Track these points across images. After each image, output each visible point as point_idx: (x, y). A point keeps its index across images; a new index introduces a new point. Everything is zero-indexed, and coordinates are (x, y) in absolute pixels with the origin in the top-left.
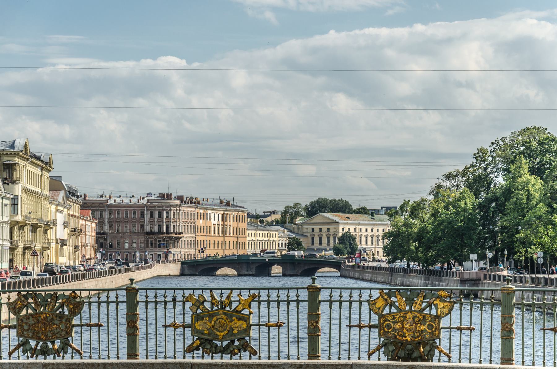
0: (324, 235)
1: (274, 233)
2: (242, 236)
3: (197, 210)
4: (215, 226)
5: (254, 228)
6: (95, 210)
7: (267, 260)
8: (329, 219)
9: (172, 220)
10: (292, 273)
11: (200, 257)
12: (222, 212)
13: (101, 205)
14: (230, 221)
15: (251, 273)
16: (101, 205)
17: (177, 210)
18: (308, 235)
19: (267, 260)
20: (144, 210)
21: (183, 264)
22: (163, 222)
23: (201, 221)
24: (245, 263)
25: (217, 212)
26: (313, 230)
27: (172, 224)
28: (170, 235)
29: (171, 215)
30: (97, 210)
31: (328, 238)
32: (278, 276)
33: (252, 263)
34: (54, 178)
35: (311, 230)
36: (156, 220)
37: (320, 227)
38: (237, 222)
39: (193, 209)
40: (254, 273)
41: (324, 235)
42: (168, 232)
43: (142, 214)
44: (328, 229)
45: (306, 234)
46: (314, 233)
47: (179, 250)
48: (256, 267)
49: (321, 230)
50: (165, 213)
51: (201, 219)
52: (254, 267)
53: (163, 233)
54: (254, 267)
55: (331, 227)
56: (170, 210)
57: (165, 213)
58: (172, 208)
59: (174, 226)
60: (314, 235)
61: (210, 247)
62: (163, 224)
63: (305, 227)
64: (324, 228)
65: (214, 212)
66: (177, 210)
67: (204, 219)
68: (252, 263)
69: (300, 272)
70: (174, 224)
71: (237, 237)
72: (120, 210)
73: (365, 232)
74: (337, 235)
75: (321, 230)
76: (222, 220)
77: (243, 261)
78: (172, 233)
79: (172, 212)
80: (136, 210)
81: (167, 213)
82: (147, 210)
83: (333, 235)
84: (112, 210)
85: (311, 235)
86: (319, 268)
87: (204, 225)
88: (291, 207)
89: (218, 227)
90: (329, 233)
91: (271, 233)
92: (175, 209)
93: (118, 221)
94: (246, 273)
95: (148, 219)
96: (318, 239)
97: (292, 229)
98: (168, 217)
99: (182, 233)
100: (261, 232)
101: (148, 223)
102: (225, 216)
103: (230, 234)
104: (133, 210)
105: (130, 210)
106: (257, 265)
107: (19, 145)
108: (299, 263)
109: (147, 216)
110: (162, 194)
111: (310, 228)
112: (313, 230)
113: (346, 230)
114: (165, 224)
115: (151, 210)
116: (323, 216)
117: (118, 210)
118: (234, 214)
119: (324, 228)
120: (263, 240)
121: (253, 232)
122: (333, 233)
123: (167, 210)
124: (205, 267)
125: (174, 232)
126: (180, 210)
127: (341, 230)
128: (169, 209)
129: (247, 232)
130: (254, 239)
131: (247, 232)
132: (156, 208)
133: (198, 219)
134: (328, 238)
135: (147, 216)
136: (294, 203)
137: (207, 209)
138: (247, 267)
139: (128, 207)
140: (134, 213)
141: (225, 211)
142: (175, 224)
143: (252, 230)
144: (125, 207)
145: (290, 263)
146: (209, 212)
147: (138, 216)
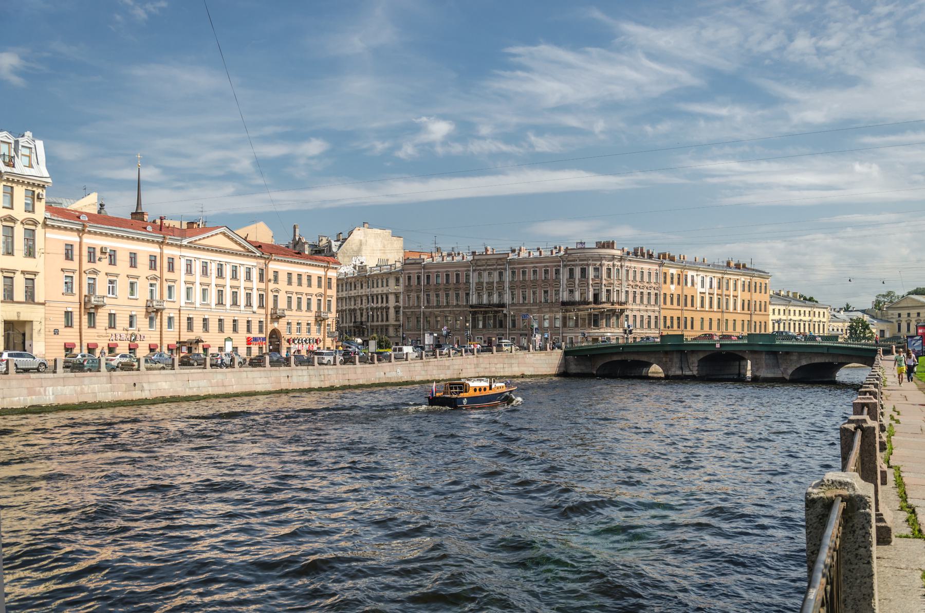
1: (822, 311)
2: (672, 307)
3: (664, 269)
4: (703, 295)
5: (784, 302)
6: (491, 269)
7: (718, 346)
8: (919, 301)
9: (604, 282)
10: (770, 375)
12: (720, 276)
13: (500, 262)
14: (735, 290)
15: (688, 373)
16: (500, 262)
17: (614, 265)
18: (894, 320)
19: (718, 346)
20: (560, 266)
21: (566, 353)
22: (588, 284)
23: (673, 287)
24: (678, 351)
25: (707, 274)
26: (899, 315)
27: (604, 289)
28: (601, 306)
29: (602, 274)
30: (495, 269)
33: (693, 352)
36: (577, 282)
37: (900, 312)
38: (749, 291)
39: (656, 267)
40: (695, 373)
42: (608, 301)
43: (557, 272)
45: (891, 320)
48: (700, 361)
49: (909, 315)
50: (591, 269)
51: (672, 283)
52: (694, 360)
53: (589, 303)
54: (696, 361)
56: (601, 265)
57: (591, 269)
58: (604, 262)
59: (608, 291)
61: (692, 328)
62: (588, 288)
63: (890, 312)
64: (913, 312)
65: (702, 274)
66: (614, 265)
67: (679, 283)
68: (693, 352)
69: (790, 372)
70: (609, 288)
71: (751, 314)
72: (525, 268)
75: (909, 315)
76: (719, 288)
78: (604, 303)
79: (604, 269)
80: (548, 266)
81: (596, 269)
82: (565, 266)
84: (515, 268)
87: (680, 293)
88: (884, 296)
89: (711, 298)
91: (817, 310)
92: (611, 263)
93: (524, 285)
94: (679, 373)
95: (565, 282)
97: (874, 314)
98: (596, 277)
99: (625, 303)
100: (797, 309)
101: (565, 286)
102: (725, 281)
103: (711, 307)
104: (545, 267)
105: (541, 268)
106: (701, 356)
107: (699, 260)
108: (787, 353)
109: (564, 276)
110: (600, 242)
114: (591, 289)
115: (569, 265)
116: (912, 299)
117: (523, 268)
118: (743, 279)
120: (801, 320)
121: (782, 308)
123: (595, 265)
124: (607, 360)
125: (608, 301)
126: (621, 266)
128: (598, 263)
129: (771, 308)
130: (784, 318)
131: (771, 308)
132: (577, 262)
133: (665, 282)
135: (564, 276)
137: (684, 268)
138: (681, 361)
139: (537, 263)
140: (546, 272)
141: (725, 274)
142: (611, 288)
143: (779, 305)
144: (532, 263)
145: (768, 353)
146: (690, 273)
147: (552, 275)
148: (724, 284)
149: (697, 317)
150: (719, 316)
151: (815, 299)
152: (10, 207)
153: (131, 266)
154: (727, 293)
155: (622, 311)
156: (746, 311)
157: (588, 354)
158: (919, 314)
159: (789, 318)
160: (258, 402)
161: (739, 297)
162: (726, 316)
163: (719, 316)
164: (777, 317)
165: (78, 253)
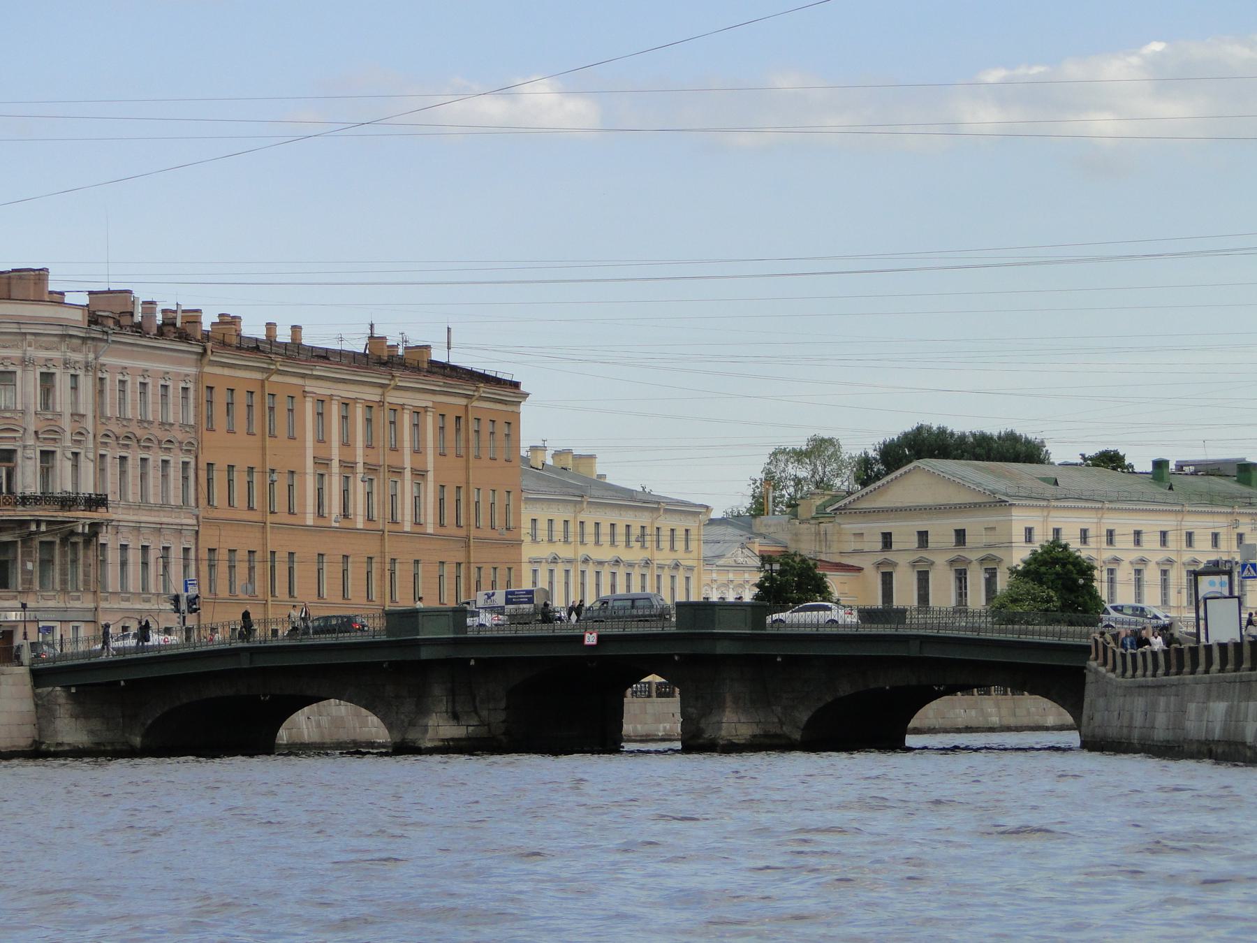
0: (940, 560)
2: (230, 514)
7: (590, 639)
11: (1244, 659)
18: (866, 563)
19: (590, 639)
26: (887, 539)
31: (961, 576)
32: (988, 749)
34: (461, 97)
35: (914, 542)
37: (959, 522)
41: (940, 560)
44: (960, 535)
46: (889, 555)
47: (87, 602)
55: (974, 525)
60: (894, 564)
73: (1157, 545)
74: (1001, 561)
77: (721, 648)
83: (982, 561)
85: (879, 565)
86: (929, 695)
88: (799, 456)
90: (924, 554)
96: (951, 578)
111: (874, 529)
112: (887, 539)
113: (1042, 538)
119: (941, 530)
122: (982, 554)
127: (1018, 535)
130: (565, 552)
134: (961, 576)
136: (810, 434)
148: (1174, 661)
149: (306, 548)
150: (371, 547)
151: (495, 425)
152: (1207, 600)
153: (890, 534)
154: (391, 459)
155: (95, 527)
156: (451, 529)
157: (122, 678)
158: (960, 535)
159: (582, 552)
160: (292, 616)
161: (430, 476)
162: (391, 548)
163: (371, 547)
164: (544, 551)
165: (200, 472)
